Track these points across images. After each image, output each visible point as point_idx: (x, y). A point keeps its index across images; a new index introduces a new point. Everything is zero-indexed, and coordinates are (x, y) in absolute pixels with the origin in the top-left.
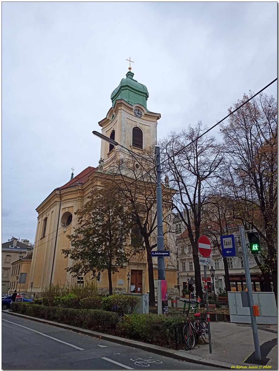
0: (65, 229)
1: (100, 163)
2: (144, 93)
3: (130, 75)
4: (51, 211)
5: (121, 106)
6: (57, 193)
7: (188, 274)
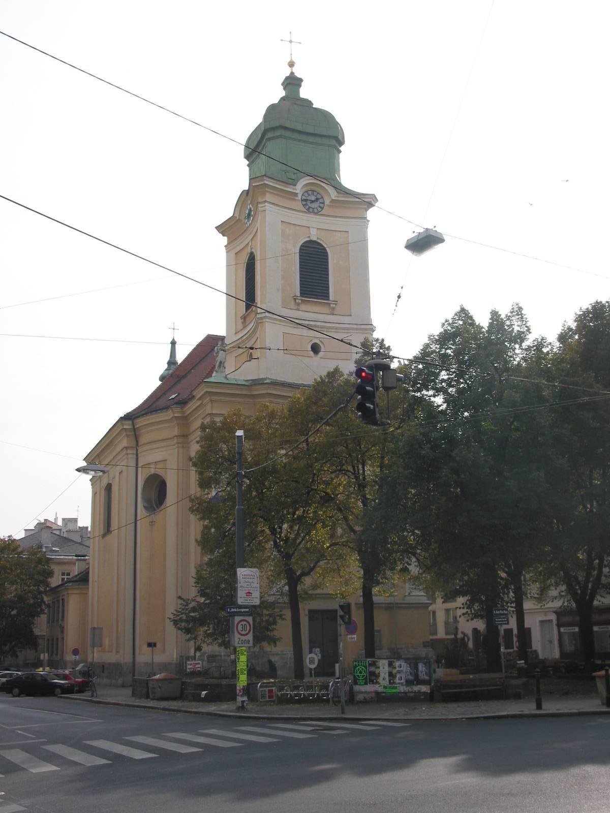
3: (292, 83)
5: (263, 194)
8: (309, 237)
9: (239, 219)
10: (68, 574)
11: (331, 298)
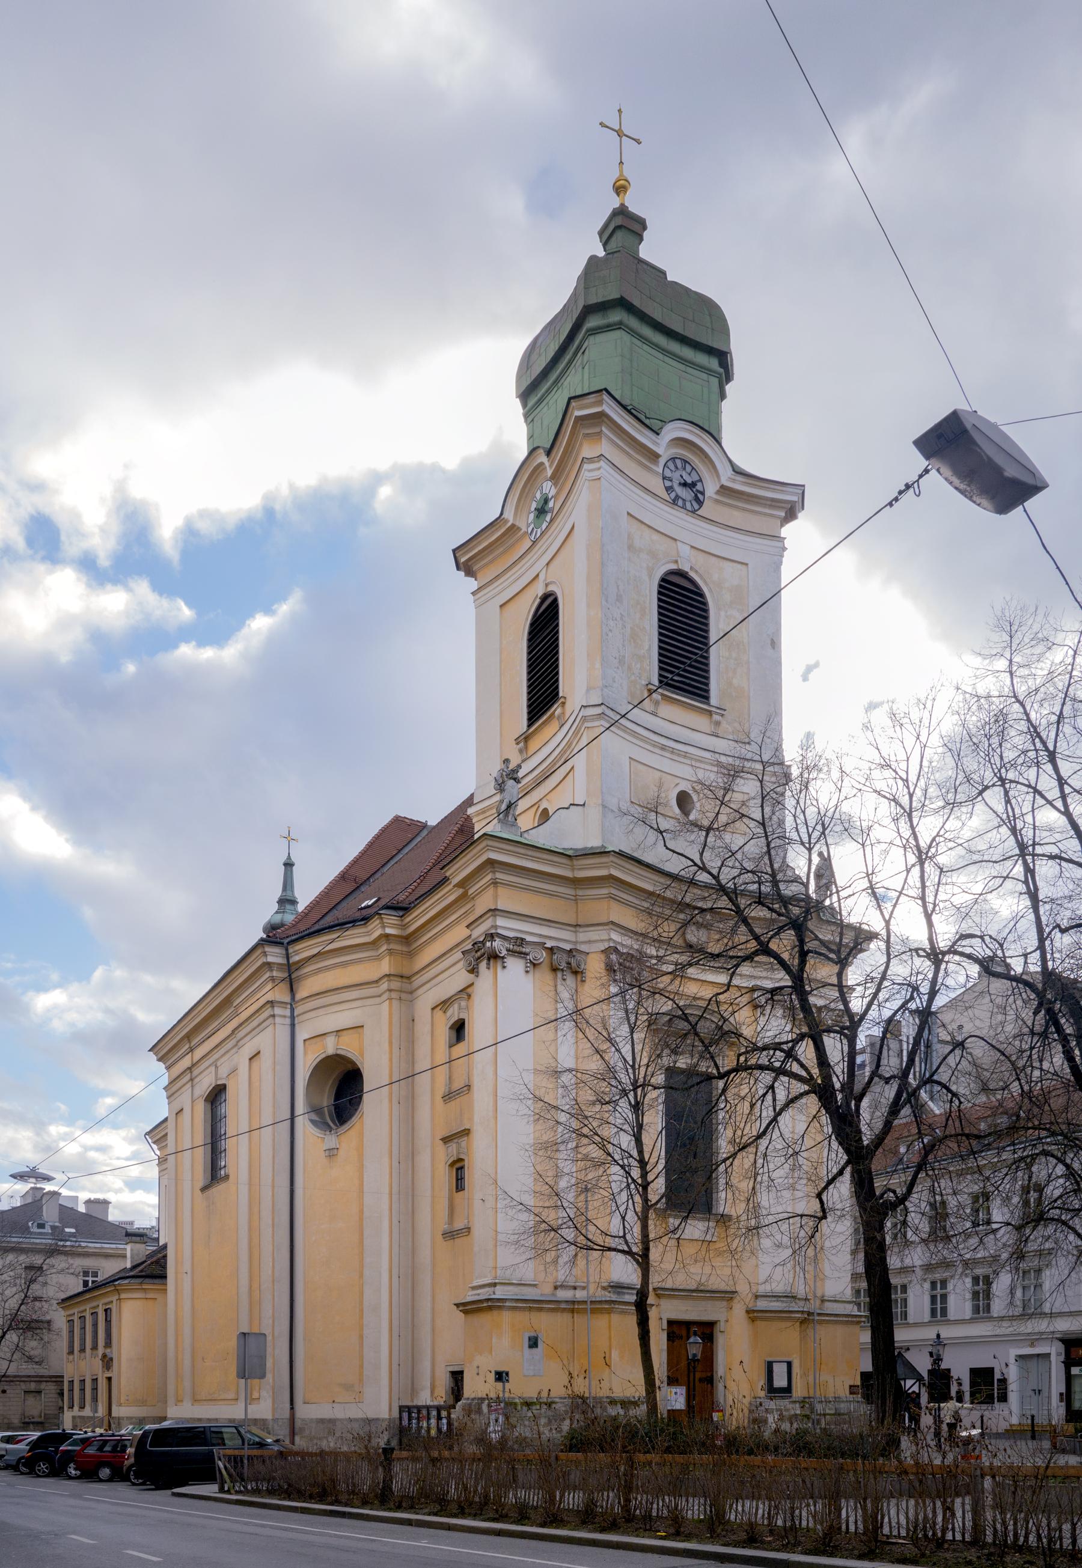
0: (331, 1140)
1: (501, 787)
2: (710, 351)
4: (248, 1050)
6: (270, 959)
7: (938, 1336)
8: (676, 562)
9: (513, 525)
10: (95, 1274)
11: (713, 701)
